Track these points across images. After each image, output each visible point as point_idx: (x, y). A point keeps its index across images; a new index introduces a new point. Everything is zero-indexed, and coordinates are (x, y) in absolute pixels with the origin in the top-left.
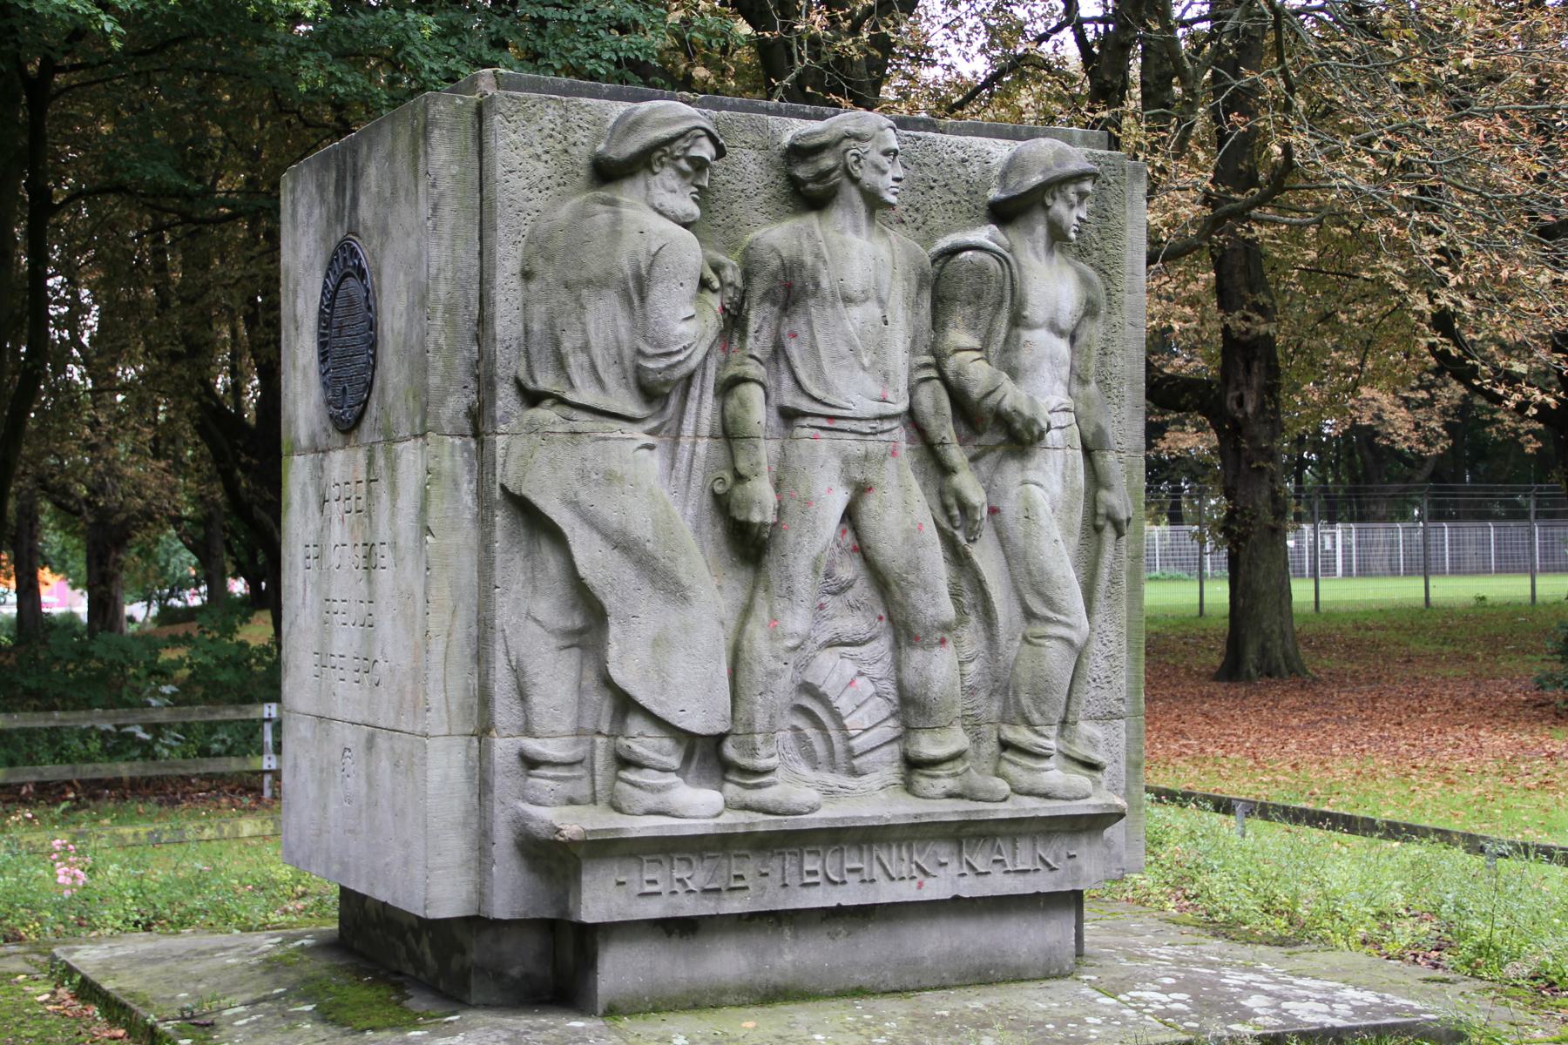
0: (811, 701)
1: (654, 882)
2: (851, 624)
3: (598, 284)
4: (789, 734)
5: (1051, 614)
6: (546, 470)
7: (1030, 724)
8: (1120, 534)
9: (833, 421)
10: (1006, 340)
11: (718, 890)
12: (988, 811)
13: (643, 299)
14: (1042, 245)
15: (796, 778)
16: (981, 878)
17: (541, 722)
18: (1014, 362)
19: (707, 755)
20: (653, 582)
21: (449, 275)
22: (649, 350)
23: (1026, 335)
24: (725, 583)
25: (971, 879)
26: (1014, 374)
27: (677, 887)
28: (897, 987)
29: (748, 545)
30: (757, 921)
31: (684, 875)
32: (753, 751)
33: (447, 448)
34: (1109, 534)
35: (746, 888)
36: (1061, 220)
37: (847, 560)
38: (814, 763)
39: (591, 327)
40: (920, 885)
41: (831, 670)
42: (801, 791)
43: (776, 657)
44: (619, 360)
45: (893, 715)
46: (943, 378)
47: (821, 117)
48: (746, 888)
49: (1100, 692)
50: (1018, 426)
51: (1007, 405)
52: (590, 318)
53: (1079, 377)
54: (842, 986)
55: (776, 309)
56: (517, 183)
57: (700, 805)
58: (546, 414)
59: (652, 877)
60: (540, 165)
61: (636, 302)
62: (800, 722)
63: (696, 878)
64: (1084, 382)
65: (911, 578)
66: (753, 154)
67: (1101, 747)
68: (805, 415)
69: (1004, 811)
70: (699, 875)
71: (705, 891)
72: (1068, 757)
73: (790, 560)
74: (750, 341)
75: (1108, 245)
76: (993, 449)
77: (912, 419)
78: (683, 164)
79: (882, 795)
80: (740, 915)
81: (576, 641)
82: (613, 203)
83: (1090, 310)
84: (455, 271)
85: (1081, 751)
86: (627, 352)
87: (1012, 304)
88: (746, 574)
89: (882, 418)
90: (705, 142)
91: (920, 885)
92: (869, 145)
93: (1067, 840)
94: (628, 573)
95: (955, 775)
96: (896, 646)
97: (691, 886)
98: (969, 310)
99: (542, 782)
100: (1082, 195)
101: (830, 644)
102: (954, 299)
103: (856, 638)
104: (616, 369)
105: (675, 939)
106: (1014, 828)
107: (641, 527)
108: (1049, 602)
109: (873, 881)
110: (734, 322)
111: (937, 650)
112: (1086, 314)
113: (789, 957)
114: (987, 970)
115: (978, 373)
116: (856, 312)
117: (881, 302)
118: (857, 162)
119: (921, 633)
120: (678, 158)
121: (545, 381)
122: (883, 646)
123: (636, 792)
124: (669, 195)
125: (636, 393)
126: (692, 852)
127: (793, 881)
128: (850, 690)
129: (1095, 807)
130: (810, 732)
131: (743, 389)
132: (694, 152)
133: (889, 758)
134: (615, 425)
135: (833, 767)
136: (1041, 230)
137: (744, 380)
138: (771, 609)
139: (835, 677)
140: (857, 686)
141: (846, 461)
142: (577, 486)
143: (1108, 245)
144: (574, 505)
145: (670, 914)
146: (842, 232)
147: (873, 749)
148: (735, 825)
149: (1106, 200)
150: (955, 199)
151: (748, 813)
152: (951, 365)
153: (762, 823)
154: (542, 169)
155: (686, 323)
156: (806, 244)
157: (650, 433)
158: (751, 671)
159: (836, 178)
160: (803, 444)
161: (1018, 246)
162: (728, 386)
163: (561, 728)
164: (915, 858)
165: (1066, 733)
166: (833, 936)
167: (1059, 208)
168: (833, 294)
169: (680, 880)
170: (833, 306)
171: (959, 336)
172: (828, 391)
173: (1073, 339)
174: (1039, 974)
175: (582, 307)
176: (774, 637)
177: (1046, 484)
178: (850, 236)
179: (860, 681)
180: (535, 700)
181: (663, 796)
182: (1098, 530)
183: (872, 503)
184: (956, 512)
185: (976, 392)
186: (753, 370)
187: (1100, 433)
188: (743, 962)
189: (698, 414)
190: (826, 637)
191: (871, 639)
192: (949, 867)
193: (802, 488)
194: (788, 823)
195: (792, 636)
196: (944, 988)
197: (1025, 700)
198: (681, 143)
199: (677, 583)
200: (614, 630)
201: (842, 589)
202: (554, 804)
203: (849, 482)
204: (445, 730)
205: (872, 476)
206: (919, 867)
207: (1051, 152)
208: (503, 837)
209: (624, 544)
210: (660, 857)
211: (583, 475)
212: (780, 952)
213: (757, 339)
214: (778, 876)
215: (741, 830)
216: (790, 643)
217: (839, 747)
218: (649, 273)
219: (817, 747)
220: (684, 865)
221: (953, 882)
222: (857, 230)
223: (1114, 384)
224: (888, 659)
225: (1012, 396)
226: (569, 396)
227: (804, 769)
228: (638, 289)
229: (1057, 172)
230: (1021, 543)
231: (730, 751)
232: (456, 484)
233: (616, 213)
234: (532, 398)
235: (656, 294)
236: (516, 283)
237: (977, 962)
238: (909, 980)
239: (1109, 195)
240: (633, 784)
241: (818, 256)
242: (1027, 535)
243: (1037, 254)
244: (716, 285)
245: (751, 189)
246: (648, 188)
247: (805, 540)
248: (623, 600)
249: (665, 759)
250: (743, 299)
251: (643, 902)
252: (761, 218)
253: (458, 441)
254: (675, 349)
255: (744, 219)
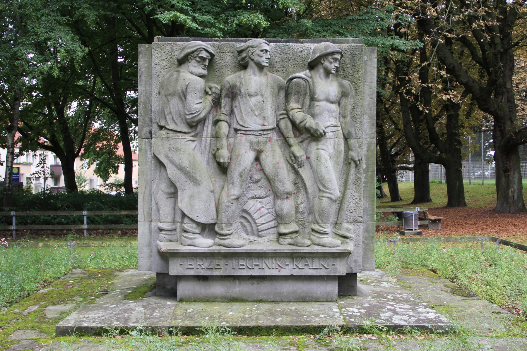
0: (246, 215)
1: (191, 265)
2: (259, 192)
3: (173, 95)
4: (240, 224)
5: (325, 190)
6: (161, 148)
7: (318, 224)
8: (357, 166)
9: (247, 132)
10: (310, 105)
11: (212, 268)
12: (301, 250)
13: (185, 98)
14: (322, 75)
15: (240, 237)
16: (301, 270)
17: (163, 219)
18: (313, 112)
19: (208, 229)
20: (190, 179)
21: (144, 94)
22: (187, 113)
23: (317, 103)
24: (217, 180)
25: (297, 270)
26: (313, 116)
27: (199, 267)
28: (274, 300)
29: (223, 169)
30: (227, 278)
31: (201, 264)
32: (222, 229)
33: (144, 142)
34: (353, 165)
35: (221, 268)
36: (327, 67)
37: (258, 173)
38: (248, 233)
39: (171, 107)
40: (279, 271)
41: (252, 206)
42: (240, 241)
43: (229, 202)
44: (180, 116)
45: (274, 219)
46: (289, 118)
47: (246, 41)
48: (221, 268)
49: (352, 214)
50: (312, 132)
51: (307, 125)
52: (171, 104)
53: (342, 116)
54: (255, 299)
55: (230, 99)
56: (158, 67)
57: (205, 243)
58: (163, 132)
59: (191, 263)
60: (164, 62)
61: (184, 99)
62: (243, 221)
63: (205, 264)
64: (344, 117)
65: (276, 178)
66: (229, 54)
67: (352, 231)
68: (239, 130)
69: (306, 250)
70: (206, 264)
71: (208, 268)
72: (336, 234)
73: (232, 173)
74: (222, 109)
75: (355, 74)
76: (307, 139)
77: (278, 129)
78: (198, 59)
79: (268, 243)
80: (222, 276)
81: (173, 196)
82: (178, 71)
83: (344, 94)
84: (146, 93)
85: (341, 232)
86: (182, 114)
87: (310, 94)
88: (223, 177)
89: (263, 130)
90: (204, 52)
91: (279, 271)
92: (256, 49)
93: (332, 260)
94: (183, 177)
95: (292, 238)
96: (274, 199)
97: (203, 267)
98: (296, 97)
99: (162, 235)
100: (336, 60)
101: (252, 198)
102: (291, 93)
103: (261, 196)
104: (180, 119)
105: (201, 282)
106: (311, 255)
107: (185, 163)
108: (324, 186)
109: (263, 269)
110: (217, 103)
111: (285, 200)
112: (342, 96)
113: (238, 289)
114: (306, 298)
115: (298, 115)
116: (253, 99)
117: (262, 96)
118: (252, 54)
119: (280, 195)
120: (196, 57)
121: (162, 123)
122: (271, 198)
123: (185, 239)
124: (194, 68)
125: (187, 125)
126: (204, 257)
127: (237, 267)
128: (259, 212)
129: (339, 250)
130: (246, 224)
131: (220, 123)
132: (200, 55)
133: (273, 232)
134: (182, 134)
135: (254, 235)
136: (322, 71)
137: (220, 121)
138: (228, 188)
139: (253, 208)
140: (261, 210)
141: (252, 144)
142: (168, 152)
143: (355, 74)
144: (167, 157)
145: (197, 274)
146: (250, 75)
147: (266, 230)
148: (214, 250)
149: (354, 60)
150: (297, 63)
151: (221, 247)
152: (291, 114)
153: (223, 249)
154: (165, 63)
155: (198, 105)
156: (237, 79)
157: (192, 136)
158: (222, 205)
159: (247, 59)
160: (238, 138)
161: (314, 76)
162: (216, 122)
163: (168, 220)
164: (278, 262)
165: (337, 227)
166: (253, 284)
167: (327, 64)
168: (245, 94)
169: (199, 265)
170: (246, 97)
171: (293, 105)
172: (245, 123)
173: (339, 104)
174: (324, 300)
175: (169, 101)
176: (228, 196)
177: (327, 149)
178: (252, 77)
179: (262, 209)
180: (161, 212)
181: (193, 241)
182: (350, 163)
183: (263, 156)
184: (293, 158)
185: (298, 122)
186: (223, 117)
187: (349, 133)
188: (223, 290)
189: (207, 131)
190: (251, 196)
191: (266, 197)
192: (290, 266)
193: (237, 152)
194: (231, 250)
195: (233, 195)
196: (290, 302)
197: (317, 216)
198: (196, 53)
199: (196, 180)
200: (179, 193)
201: (257, 182)
202: (165, 241)
203: (254, 150)
204: (143, 220)
205: (262, 148)
206: (279, 265)
207: (323, 46)
208: (155, 250)
209: (181, 169)
210: (193, 258)
211: (170, 149)
212: (235, 288)
213: (224, 108)
214: (231, 265)
215: (216, 251)
216: (233, 197)
217: (254, 228)
218: (186, 91)
219: (248, 228)
220: (243, 261)
221: (291, 270)
222: (255, 74)
223: (358, 117)
224: (272, 203)
225: (310, 122)
226: (168, 127)
227: (244, 235)
228: (183, 95)
229: (324, 52)
230: (315, 168)
231: (216, 229)
232: (146, 152)
233: (179, 74)
234: (161, 128)
235: (188, 97)
236: (157, 95)
237: (302, 295)
238: (278, 299)
239: (356, 58)
240: (185, 237)
241: (241, 83)
242: (317, 165)
243: (321, 78)
244: (210, 93)
245: (228, 65)
246: (188, 67)
247: (237, 167)
248: (181, 185)
249: (194, 230)
250: (220, 97)
251: (188, 270)
252: (230, 73)
253: (147, 140)
254: (194, 112)
255: (224, 73)
